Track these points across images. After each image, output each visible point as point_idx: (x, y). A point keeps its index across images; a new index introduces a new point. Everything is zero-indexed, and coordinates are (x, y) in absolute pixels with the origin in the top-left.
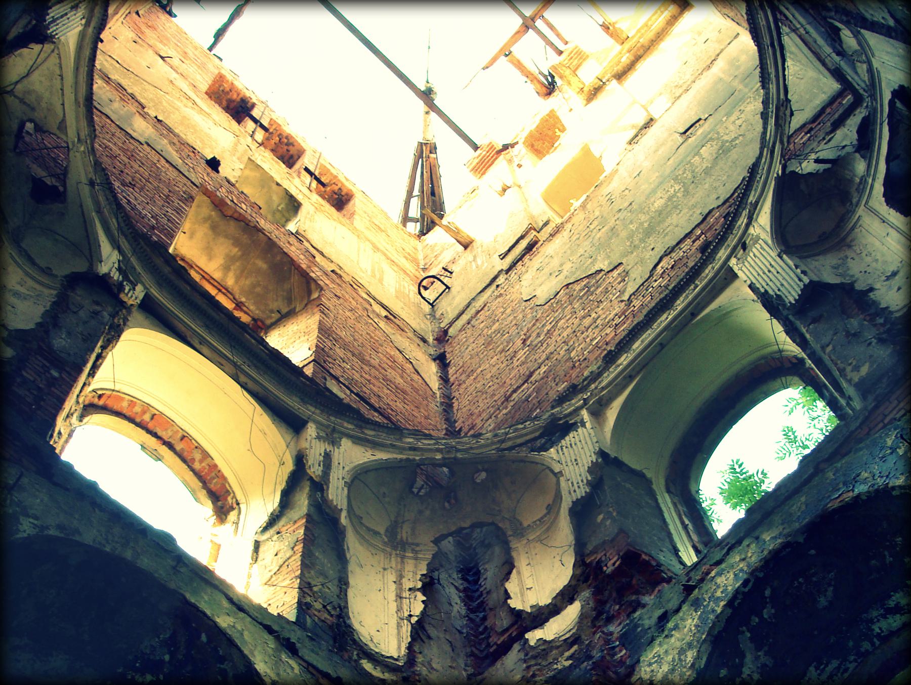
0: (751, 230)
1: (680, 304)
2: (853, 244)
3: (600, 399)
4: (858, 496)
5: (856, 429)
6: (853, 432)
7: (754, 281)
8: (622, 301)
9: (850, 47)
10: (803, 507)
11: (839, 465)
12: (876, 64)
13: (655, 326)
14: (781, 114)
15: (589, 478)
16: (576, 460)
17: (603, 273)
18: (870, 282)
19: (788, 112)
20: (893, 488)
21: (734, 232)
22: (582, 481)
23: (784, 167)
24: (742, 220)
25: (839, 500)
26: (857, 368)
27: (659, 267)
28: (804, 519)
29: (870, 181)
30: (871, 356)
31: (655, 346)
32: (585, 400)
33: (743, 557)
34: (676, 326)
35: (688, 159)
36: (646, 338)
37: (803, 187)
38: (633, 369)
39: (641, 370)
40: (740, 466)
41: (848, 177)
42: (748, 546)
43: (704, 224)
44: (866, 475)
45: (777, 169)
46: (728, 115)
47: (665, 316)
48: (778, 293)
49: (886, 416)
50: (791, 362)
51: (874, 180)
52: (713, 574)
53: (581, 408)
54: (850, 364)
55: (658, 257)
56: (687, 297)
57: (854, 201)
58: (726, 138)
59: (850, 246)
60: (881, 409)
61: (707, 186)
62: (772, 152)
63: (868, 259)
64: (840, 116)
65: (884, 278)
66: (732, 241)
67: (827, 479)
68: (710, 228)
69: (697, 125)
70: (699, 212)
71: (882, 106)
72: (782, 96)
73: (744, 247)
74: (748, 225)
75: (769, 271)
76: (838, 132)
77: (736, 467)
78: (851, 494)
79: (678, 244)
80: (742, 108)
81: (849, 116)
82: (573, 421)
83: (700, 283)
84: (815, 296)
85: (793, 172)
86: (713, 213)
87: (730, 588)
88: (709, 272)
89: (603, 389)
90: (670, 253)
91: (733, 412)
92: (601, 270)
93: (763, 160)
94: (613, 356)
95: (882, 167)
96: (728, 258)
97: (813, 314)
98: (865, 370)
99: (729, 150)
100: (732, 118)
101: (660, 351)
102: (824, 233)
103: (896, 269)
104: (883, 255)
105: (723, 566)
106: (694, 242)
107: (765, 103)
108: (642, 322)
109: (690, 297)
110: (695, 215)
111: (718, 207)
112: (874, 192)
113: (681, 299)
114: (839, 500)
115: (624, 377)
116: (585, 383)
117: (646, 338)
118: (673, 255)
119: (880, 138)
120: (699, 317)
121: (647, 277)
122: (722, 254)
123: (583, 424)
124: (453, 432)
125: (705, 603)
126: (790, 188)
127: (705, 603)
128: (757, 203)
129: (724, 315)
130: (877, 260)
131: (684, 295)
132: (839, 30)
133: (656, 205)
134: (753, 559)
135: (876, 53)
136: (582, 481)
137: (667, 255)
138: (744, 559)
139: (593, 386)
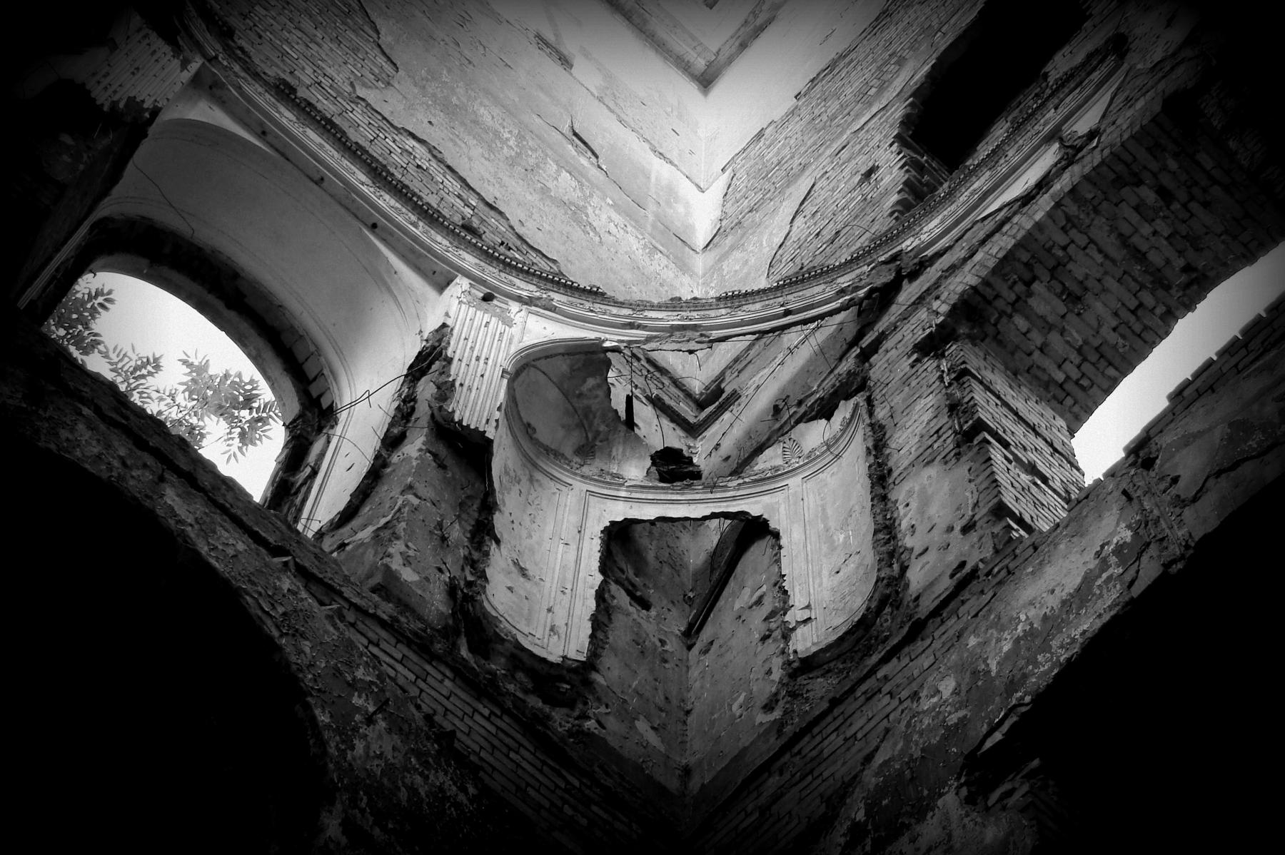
0: (514, 306)
1: (387, 202)
2: (536, 484)
3: (221, 86)
4: (279, 648)
5: (346, 599)
6: (340, 594)
7: (455, 332)
8: (352, 85)
9: (802, 435)
10: (231, 552)
11: (304, 594)
12: (794, 482)
13: (346, 162)
14: (689, 334)
15: (121, 105)
16: (138, 69)
17: (375, 36)
18: (505, 536)
19: (693, 345)
20: (307, 707)
21: (503, 275)
22: (115, 92)
23: (615, 350)
24: (526, 288)
25: (260, 613)
26: (407, 561)
27: (412, 142)
28: (217, 559)
29: (623, 494)
30: (427, 579)
31: (318, 171)
32: (216, 58)
33: (129, 462)
34: (354, 201)
35: (549, 152)
36: (326, 152)
37: (591, 382)
38: (277, 137)
39: (277, 150)
40: (101, 305)
41: (614, 453)
42: (145, 466)
43: (487, 209)
44: (307, 650)
45: (611, 338)
46: (615, 206)
47: (363, 178)
48: (457, 384)
49: (377, 645)
50: (320, 396)
51: (627, 499)
52: (86, 411)
53: (204, 55)
54: (407, 546)
55: (425, 138)
56: (400, 213)
57: (586, 470)
58: (590, 210)
59: (531, 480)
60: (383, 634)
61: (529, 197)
62: (631, 326)
63: (527, 519)
64: (669, 407)
65: (515, 556)
66: (492, 274)
67: (279, 579)
68: (482, 221)
69: (589, 154)
70: (498, 195)
71: (734, 498)
72: (716, 334)
73: (487, 298)
74: (519, 299)
75: (478, 359)
76: (650, 408)
77: (100, 300)
78: (276, 633)
79: (449, 167)
80: (629, 229)
81: (672, 421)
82: (181, 43)
83: (421, 230)
84: (464, 450)
85: (608, 364)
86: (502, 221)
87: (78, 453)
88: (440, 242)
89: (239, 88)
90: (435, 157)
91: (220, 305)
92: (378, 33)
93: (615, 310)
94: (288, 95)
95: (649, 512)
96: (467, 275)
97: (442, 450)
98: (408, 575)
99: (579, 222)
100: (615, 216)
101: (312, 180)
102: (534, 430)
103: (530, 573)
104: (539, 544)
105: (102, 427)
106: (459, 196)
107: (695, 304)
108: (348, 139)
109: (400, 219)
110: (491, 188)
111: (512, 227)
112: (610, 504)
113: (393, 202)
114: (260, 613)
115: (262, 124)
116: (239, 52)
117: (326, 152)
118: (434, 163)
119: (689, 502)
120: (372, 237)
121: (396, 124)
122: (469, 260)
123: (185, 64)
124: (487, 92)
125: (41, 412)
126: (589, 360)
127: (41, 412)
128: (553, 309)
129: (384, 282)
130: (530, 536)
131: (398, 205)
132: (828, 417)
133: (482, 110)
134: (132, 482)
135: (811, 484)
136: (115, 92)
137: (430, 151)
138: (124, 464)
139: (237, 68)
